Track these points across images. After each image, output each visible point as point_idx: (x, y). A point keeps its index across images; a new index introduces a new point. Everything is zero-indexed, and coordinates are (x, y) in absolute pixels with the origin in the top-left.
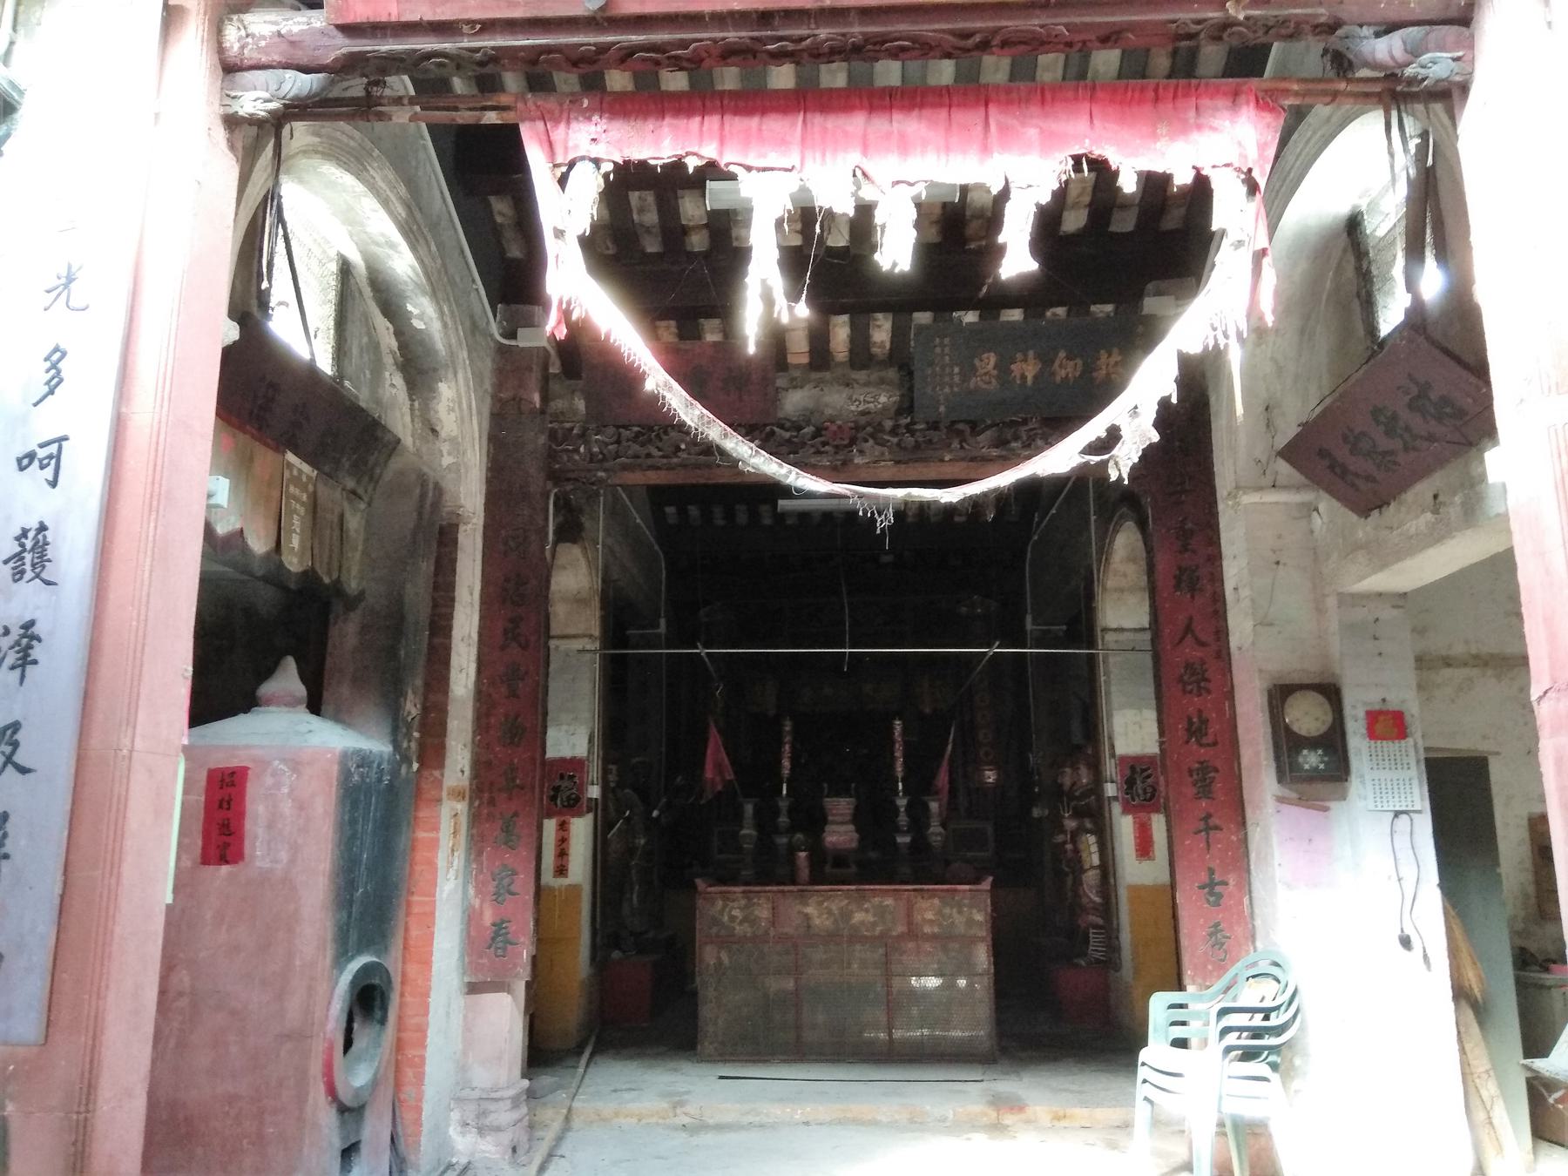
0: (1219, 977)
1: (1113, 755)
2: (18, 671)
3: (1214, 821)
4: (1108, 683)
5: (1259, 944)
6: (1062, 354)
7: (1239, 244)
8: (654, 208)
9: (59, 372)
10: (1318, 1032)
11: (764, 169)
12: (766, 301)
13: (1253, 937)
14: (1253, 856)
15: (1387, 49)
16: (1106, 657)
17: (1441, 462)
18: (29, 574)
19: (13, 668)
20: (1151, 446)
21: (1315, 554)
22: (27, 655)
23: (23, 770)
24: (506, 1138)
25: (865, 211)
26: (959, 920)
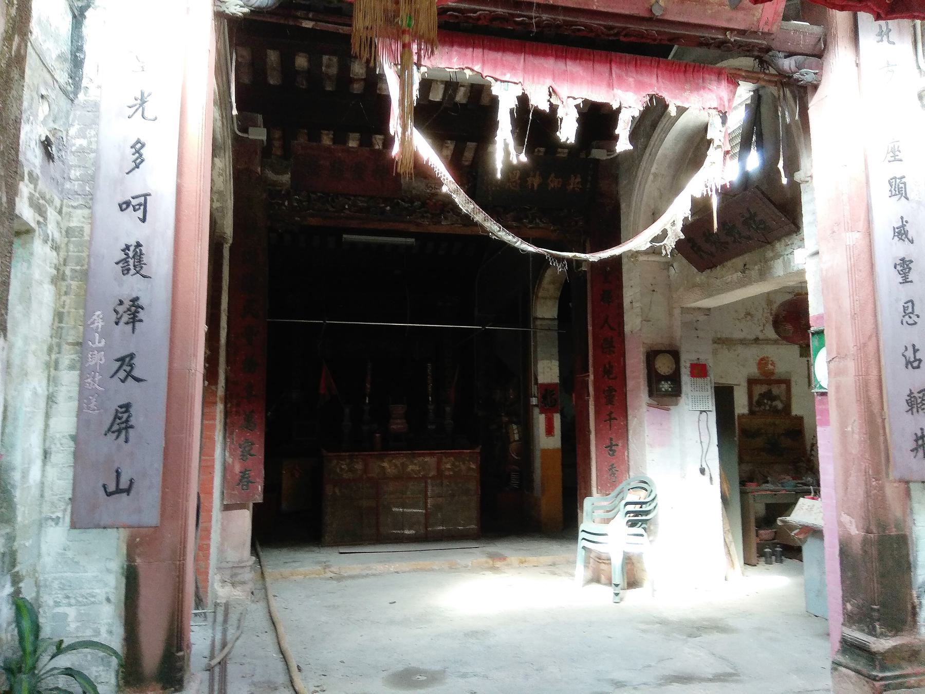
0: (613, 490)
1: (536, 383)
2: (130, 326)
3: (613, 416)
4: (536, 347)
5: (631, 473)
6: (553, 175)
7: (719, 146)
8: (336, 65)
9: (141, 155)
10: (662, 514)
11: (504, 81)
12: (505, 151)
13: (628, 471)
14: (631, 433)
15: (788, 64)
16: (535, 333)
17: (750, 249)
18: (132, 271)
19: (127, 323)
20: (680, 240)
21: (670, 287)
22: (135, 316)
23: (138, 380)
24: (248, 587)
25: (554, 108)
26: (463, 467)
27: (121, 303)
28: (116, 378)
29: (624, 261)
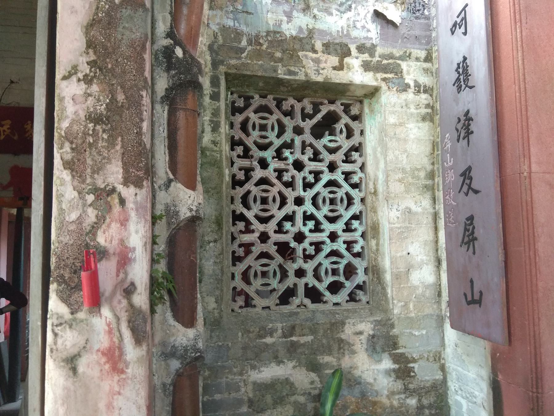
18: (463, 86)
23: (476, 192)
27: (459, 120)
28: (462, 192)
29: (2, 402)
